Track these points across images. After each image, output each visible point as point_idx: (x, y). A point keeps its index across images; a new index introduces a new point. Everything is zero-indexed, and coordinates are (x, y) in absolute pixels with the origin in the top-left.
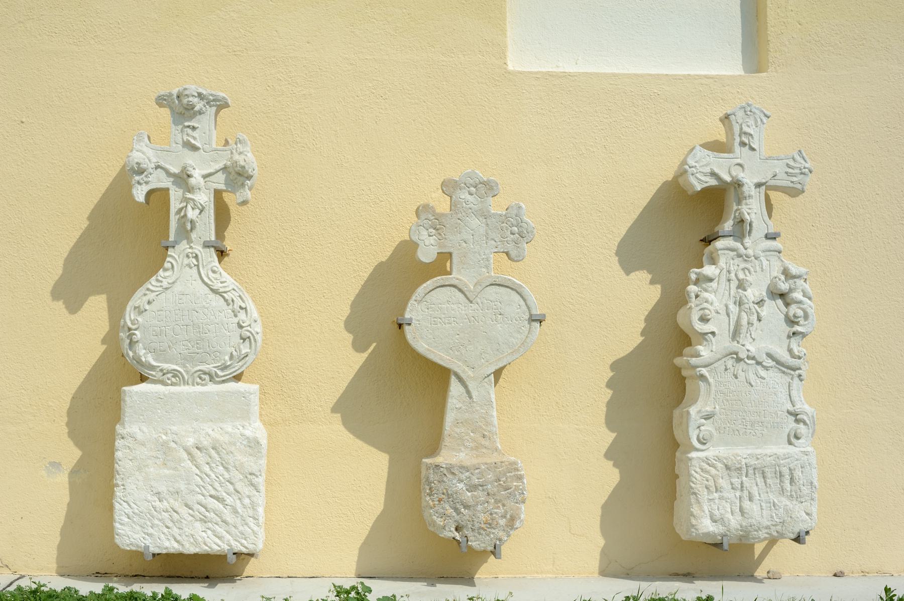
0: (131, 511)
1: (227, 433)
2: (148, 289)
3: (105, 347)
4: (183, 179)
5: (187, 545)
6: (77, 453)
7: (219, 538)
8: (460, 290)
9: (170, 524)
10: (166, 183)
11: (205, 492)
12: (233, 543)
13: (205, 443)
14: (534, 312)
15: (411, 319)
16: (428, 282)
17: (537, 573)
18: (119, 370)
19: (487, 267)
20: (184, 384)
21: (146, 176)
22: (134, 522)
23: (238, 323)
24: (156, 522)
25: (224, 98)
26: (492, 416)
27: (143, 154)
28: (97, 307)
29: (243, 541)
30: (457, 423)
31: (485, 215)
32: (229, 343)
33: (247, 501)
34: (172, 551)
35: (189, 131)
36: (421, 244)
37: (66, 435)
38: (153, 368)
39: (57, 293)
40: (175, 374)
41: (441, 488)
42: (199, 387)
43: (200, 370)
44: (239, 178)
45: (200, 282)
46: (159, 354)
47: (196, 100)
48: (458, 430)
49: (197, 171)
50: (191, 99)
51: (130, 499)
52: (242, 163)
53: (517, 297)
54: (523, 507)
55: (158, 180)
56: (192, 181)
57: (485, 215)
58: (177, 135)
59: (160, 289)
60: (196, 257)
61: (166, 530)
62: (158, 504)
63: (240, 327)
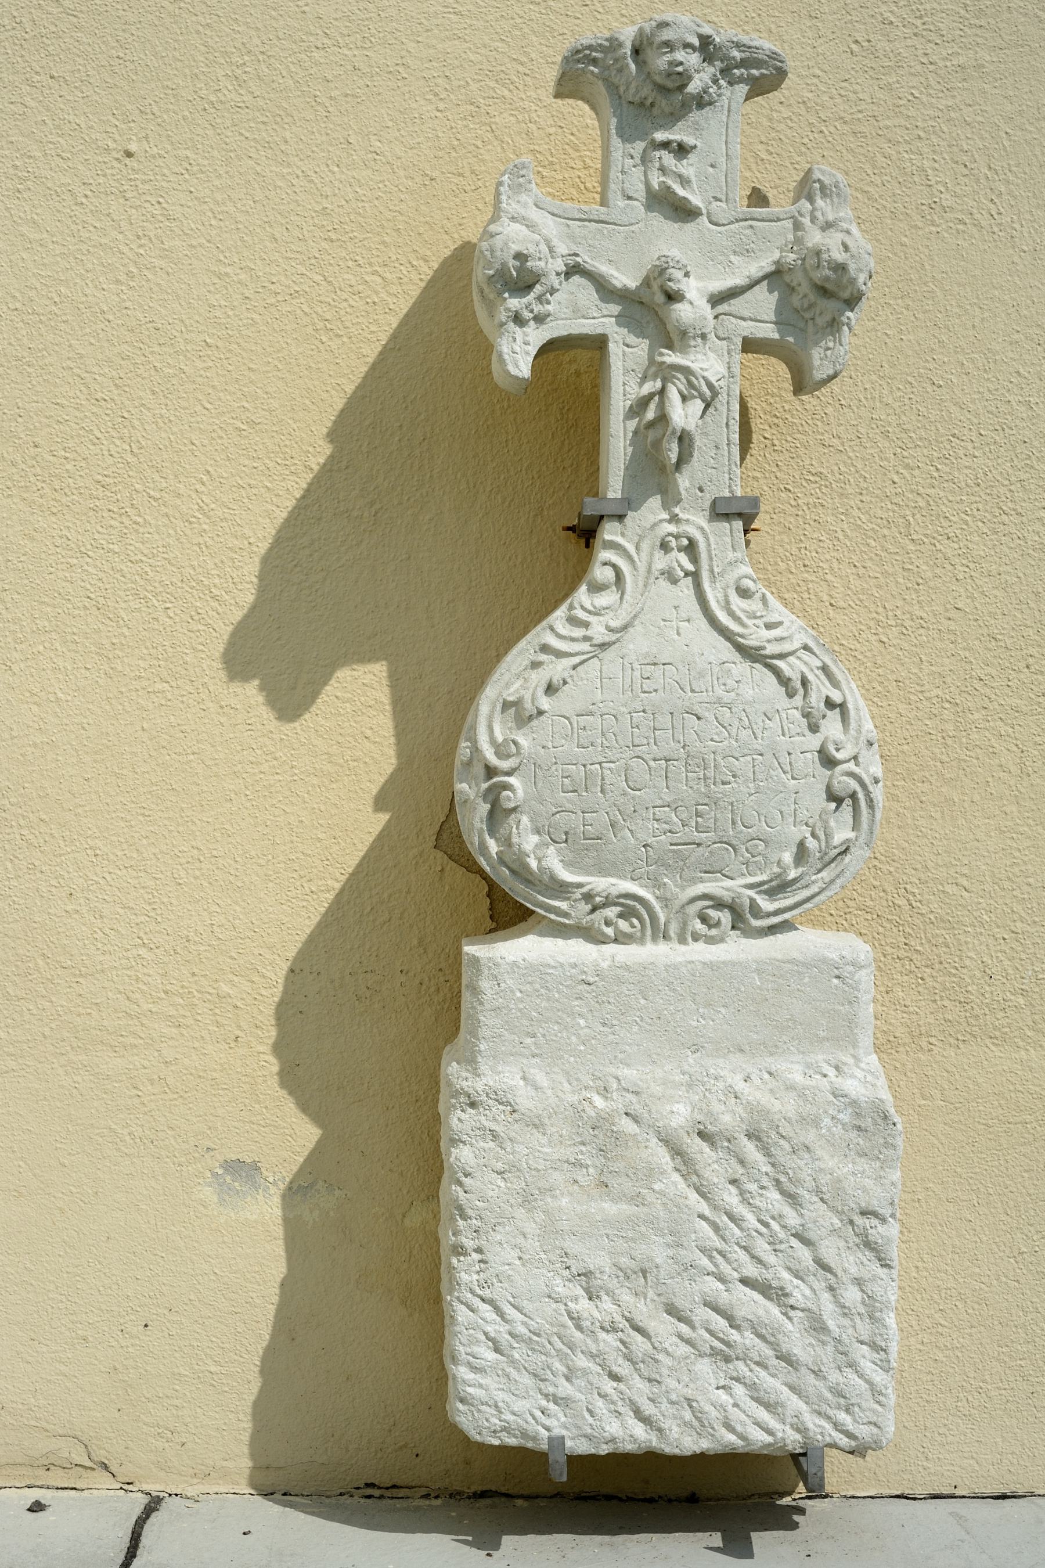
0: (503, 1328)
1: (791, 1087)
2: (545, 648)
3: (384, 817)
4: (650, 306)
5: (674, 1431)
6: (307, 1134)
7: (768, 1406)
9: (623, 1368)
10: (597, 319)
11: (726, 1269)
12: (811, 1421)
13: (727, 1118)
18: (445, 889)
20: (655, 938)
21: (539, 299)
22: (513, 1362)
23: (822, 752)
24: (582, 1362)
25: (774, 56)
27: (532, 228)
28: (359, 702)
29: (842, 1416)
32: (790, 809)
33: (852, 1295)
34: (629, 1447)
35: (669, 159)
37: (274, 1082)
38: (562, 889)
39: (238, 661)
40: (630, 907)
42: (700, 946)
43: (705, 897)
44: (824, 304)
45: (703, 624)
46: (580, 846)
47: (693, 59)
49: (692, 281)
50: (680, 55)
51: (499, 1292)
52: (839, 256)
55: (575, 311)
56: (682, 312)
58: (632, 176)
59: (585, 647)
60: (691, 549)
61: (609, 1386)
62: (583, 1306)
63: (829, 762)
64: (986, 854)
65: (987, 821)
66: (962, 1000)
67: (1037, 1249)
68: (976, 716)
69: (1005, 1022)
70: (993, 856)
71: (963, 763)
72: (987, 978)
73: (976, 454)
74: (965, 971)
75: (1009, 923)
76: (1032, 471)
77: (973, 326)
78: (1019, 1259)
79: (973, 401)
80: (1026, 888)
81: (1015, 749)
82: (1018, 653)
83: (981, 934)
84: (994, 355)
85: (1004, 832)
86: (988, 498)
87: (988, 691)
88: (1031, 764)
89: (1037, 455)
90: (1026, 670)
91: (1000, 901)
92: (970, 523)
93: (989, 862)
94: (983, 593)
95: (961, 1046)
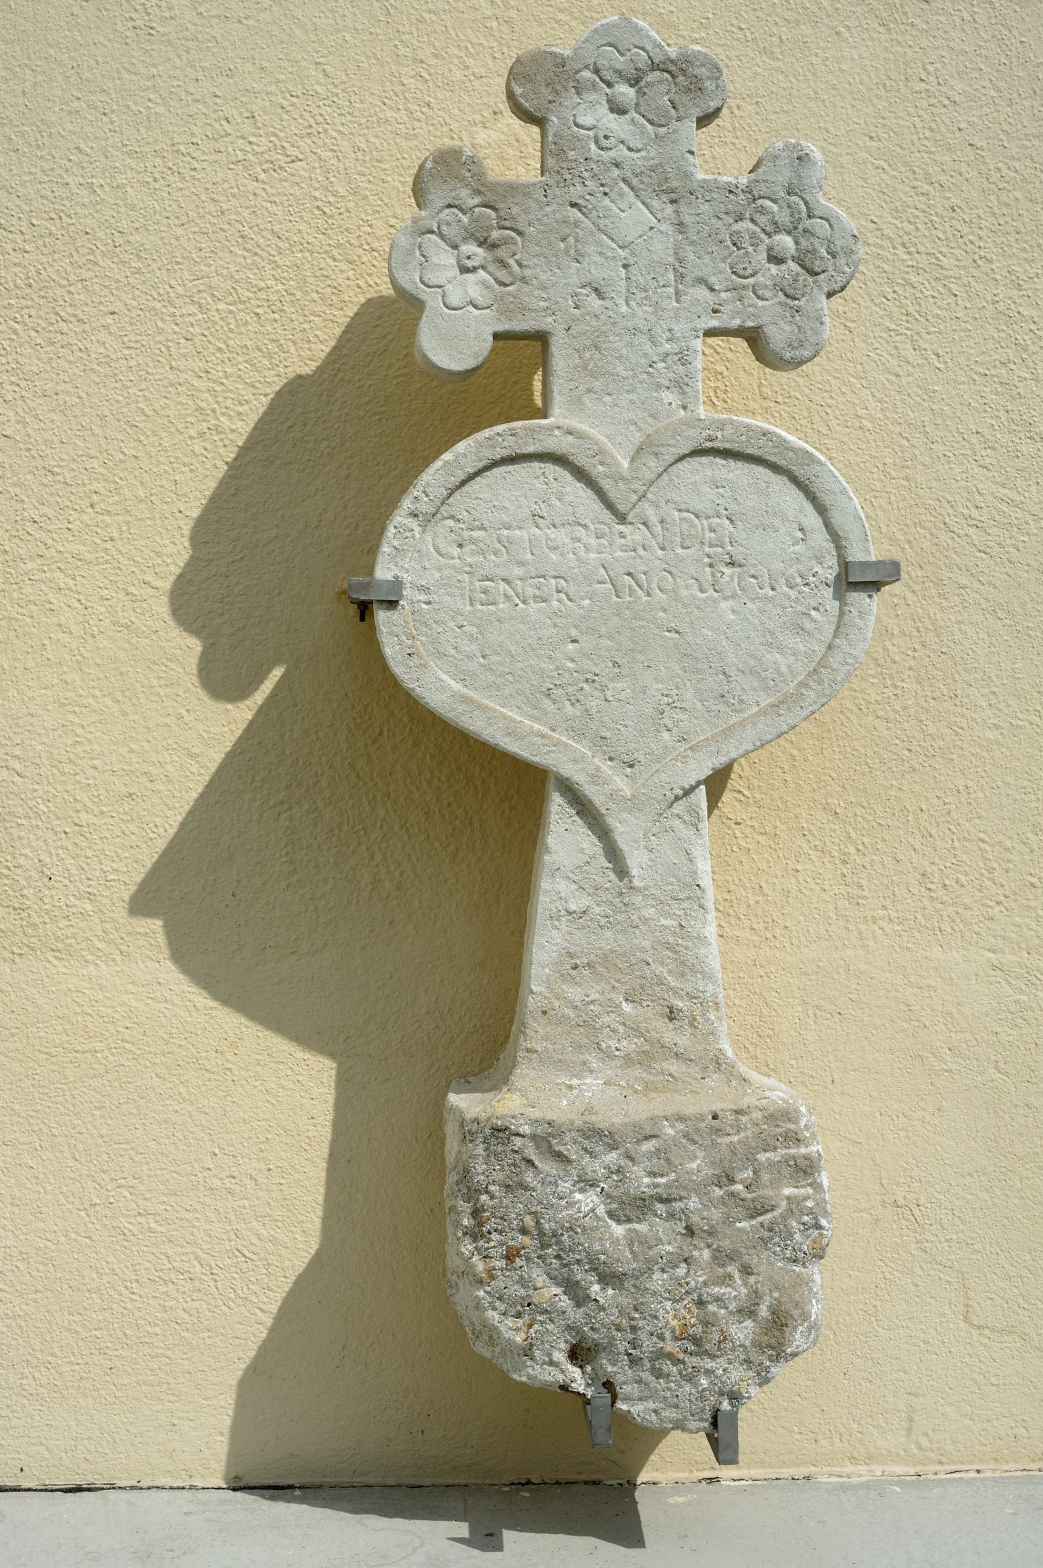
8: (581, 474)
14: (856, 554)
15: (397, 584)
16: (461, 446)
17: (853, 1459)
19: (680, 385)
26: (702, 940)
30: (572, 966)
31: (671, 189)
36: (433, 300)
41: (517, 1208)
48: (575, 993)
53: (791, 499)
54: (816, 1273)
57: (671, 189)
64: (43, 731)
65: (44, 691)
66: (17, 906)
67: (112, 1200)
68: (30, 565)
69: (69, 932)
70: (51, 733)
71: (13, 623)
72: (46, 880)
73: (27, 248)
74: (19, 871)
75: (71, 813)
76: (96, 268)
77: (24, 92)
78: (90, 1212)
79: (23, 184)
80: (91, 772)
81: (77, 604)
82: (80, 489)
83: (37, 826)
84: (49, 128)
85: (64, 705)
86: (42, 302)
87: (43, 535)
88: (96, 622)
89: (103, 248)
90: (90, 510)
91: (60, 788)
92: (21, 332)
93: (46, 741)
94: (36, 417)
95: (17, 960)
